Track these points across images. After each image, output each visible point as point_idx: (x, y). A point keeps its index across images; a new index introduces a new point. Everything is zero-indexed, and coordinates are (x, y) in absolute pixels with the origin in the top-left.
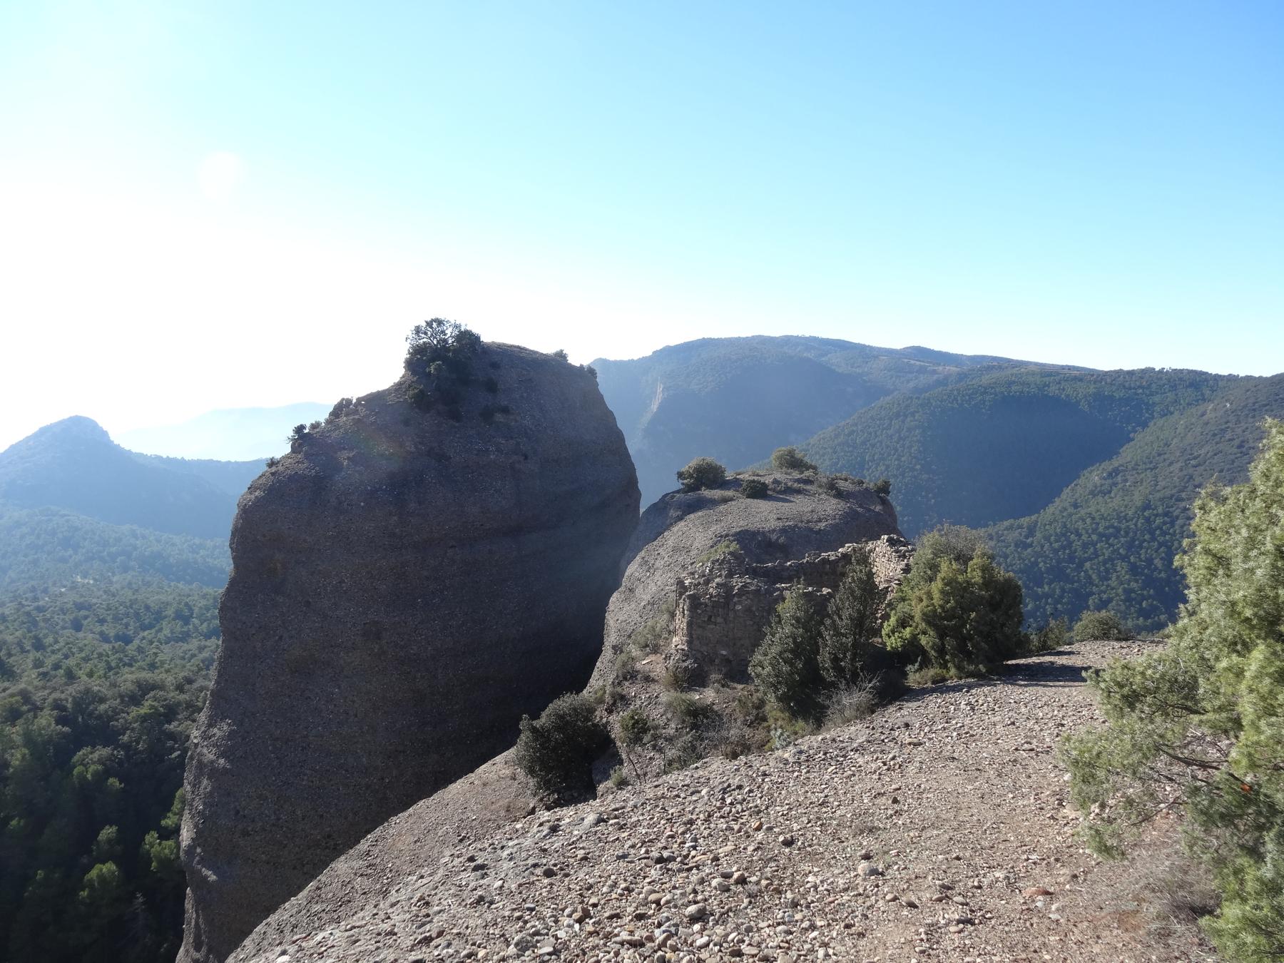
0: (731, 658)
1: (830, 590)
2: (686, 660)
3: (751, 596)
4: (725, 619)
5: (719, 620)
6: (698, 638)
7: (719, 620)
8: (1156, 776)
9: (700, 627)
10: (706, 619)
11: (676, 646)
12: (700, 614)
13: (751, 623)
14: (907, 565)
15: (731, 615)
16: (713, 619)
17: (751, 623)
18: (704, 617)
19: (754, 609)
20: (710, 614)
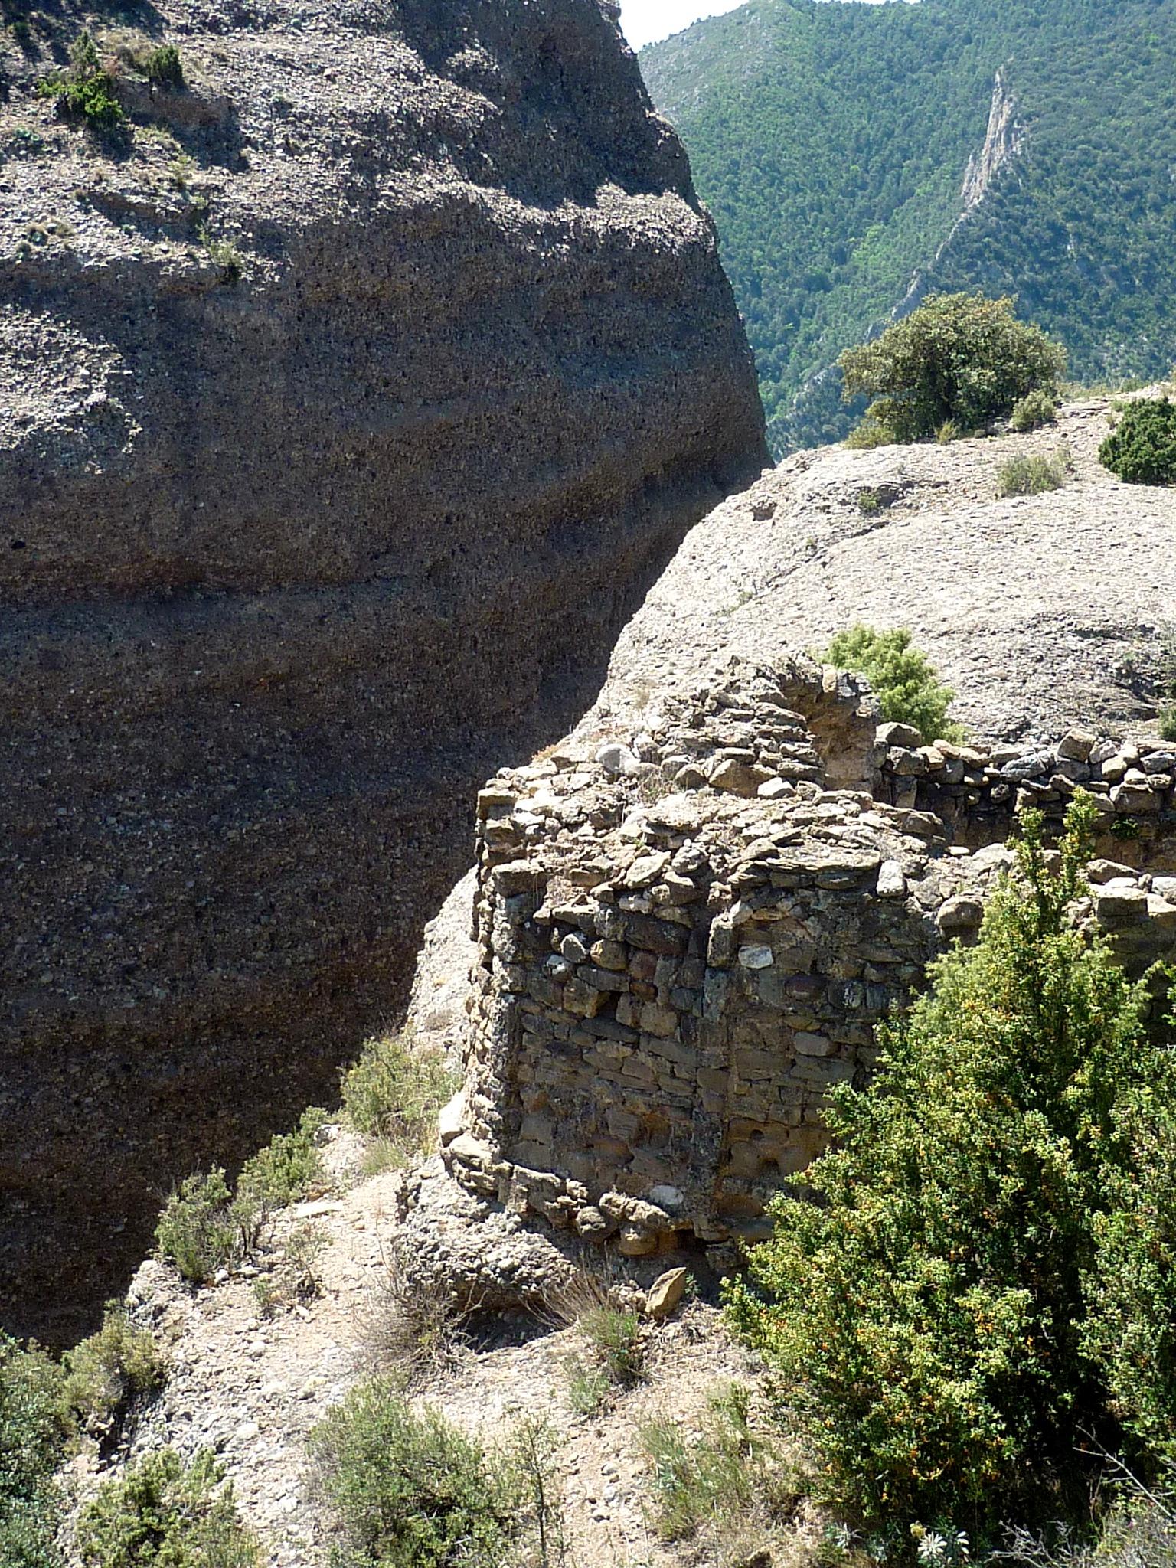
0: (702, 1226)
1: (878, 1059)
2: (482, 1217)
3: (825, 904)
4: (682, 1015)
5: (655, 1019)
6: (545, 1108)
7: (655, 1019)
8: (768, 673)
9: (558, 1048)
10: (589, 1010)
11: (448, 1139)
12: (562, 981)
13: (823, 1047)
14: (446, 1145)
15: (716, 997)
16: (624, 1014)
17: (823, 1047)
18: (581, 996)
19: (838, 971)
20: (608, 981)
